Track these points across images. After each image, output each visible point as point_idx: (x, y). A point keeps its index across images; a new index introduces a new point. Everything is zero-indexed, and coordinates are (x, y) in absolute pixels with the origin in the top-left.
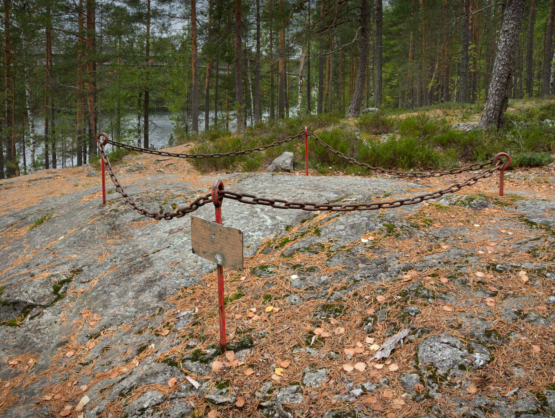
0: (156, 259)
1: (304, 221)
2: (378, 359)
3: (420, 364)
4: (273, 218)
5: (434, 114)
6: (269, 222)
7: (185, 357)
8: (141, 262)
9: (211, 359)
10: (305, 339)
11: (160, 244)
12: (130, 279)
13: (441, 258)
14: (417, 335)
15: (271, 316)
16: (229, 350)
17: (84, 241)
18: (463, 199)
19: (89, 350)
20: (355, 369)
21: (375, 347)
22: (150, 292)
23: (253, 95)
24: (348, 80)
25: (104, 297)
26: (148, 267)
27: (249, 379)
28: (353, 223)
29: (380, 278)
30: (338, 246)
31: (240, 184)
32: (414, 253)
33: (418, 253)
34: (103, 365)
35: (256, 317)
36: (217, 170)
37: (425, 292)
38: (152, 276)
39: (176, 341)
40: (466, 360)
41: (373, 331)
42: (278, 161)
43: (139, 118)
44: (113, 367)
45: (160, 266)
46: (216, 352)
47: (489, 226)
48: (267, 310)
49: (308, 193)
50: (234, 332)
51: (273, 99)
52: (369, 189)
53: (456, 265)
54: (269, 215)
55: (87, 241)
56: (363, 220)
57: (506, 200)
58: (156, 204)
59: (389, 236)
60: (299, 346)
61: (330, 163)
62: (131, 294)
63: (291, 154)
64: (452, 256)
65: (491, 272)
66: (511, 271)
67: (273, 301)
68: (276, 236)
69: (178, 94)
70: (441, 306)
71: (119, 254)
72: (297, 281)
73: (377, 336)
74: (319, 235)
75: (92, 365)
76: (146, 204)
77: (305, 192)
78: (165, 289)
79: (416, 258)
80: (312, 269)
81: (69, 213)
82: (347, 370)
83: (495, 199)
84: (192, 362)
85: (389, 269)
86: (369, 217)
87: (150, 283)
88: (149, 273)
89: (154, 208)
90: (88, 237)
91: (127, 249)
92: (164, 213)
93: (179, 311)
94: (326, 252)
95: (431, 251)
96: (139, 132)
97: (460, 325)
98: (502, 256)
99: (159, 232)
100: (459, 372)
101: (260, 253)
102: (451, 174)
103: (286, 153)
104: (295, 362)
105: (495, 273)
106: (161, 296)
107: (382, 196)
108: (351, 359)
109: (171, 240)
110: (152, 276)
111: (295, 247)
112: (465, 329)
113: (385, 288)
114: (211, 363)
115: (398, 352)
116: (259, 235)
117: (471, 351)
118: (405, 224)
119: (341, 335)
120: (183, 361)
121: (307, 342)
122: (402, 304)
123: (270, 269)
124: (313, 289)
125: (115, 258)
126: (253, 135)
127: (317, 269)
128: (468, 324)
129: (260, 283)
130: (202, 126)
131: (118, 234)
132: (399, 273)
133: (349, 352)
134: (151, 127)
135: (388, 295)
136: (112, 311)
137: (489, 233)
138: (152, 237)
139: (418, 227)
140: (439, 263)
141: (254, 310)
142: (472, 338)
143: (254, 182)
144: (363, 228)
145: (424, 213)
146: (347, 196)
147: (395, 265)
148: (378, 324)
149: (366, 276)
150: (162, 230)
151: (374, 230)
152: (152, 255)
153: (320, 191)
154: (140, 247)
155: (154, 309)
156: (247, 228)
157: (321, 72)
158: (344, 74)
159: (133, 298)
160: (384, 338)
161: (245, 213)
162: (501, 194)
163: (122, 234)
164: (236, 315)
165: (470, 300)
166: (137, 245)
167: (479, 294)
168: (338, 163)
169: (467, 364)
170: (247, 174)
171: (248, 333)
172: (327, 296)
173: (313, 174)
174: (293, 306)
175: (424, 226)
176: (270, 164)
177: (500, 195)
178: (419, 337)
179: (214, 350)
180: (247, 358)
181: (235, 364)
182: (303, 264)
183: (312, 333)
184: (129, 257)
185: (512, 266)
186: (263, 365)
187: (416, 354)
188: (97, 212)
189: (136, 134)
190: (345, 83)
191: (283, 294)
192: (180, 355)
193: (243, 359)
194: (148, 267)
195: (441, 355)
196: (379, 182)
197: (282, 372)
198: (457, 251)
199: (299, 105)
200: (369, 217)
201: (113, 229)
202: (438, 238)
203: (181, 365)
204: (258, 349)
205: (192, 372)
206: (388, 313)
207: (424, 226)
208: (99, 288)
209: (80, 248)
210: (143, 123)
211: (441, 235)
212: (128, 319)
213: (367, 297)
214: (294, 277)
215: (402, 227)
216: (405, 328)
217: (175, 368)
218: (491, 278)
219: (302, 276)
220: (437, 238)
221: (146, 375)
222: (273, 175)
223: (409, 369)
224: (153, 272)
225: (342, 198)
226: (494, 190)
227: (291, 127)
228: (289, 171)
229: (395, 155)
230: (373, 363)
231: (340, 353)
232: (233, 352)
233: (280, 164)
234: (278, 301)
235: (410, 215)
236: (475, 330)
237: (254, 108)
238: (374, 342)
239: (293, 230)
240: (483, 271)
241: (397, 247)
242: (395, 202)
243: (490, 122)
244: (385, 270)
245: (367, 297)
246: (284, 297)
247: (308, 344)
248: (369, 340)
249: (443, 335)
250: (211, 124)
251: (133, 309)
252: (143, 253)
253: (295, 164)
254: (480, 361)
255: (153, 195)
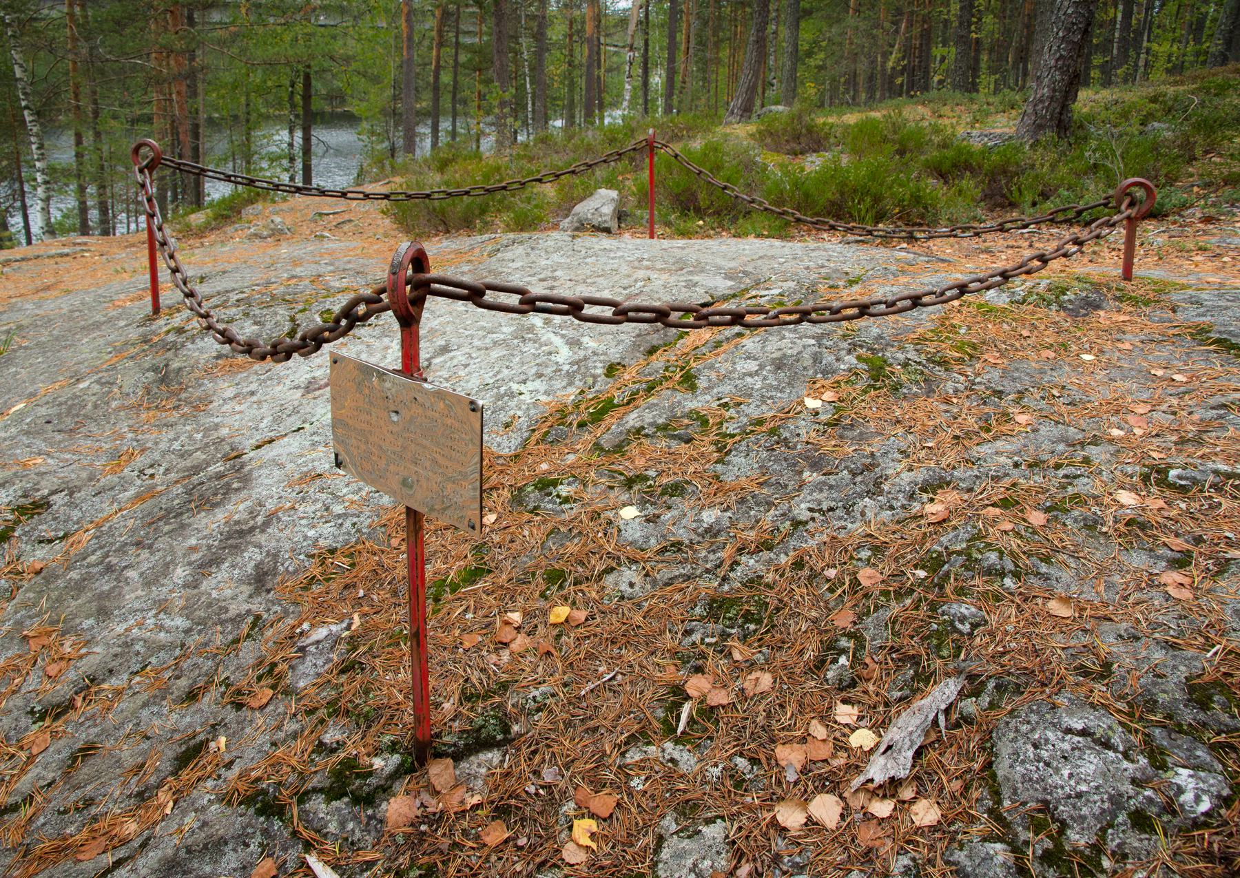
0: (261, 467)
1: (652, 351)
2: (875, 784)
3: (1007, 803)
4: (574, 343)
5: (916, 114)
6: (564, 354)
7: (309, 785)
8: (220, 476)
9: (385, 790)
10: (660, 713)
11: (277, 420)
12: (183, 526)
13: (1018, 453)
14: (985, 700)
15: (564, 638)
16: (439, 755)
17: (77, 415)
18: (1041, 289)
19: (31, 759)
20: (809, 818)
21: (862, 738)
22: (233, 566)
23: (531, 84)
24: (725, 54)
25: (105, 585)
26: (237, 490)
27: (494, 858)
28: (778, 354)
29: (863, 514)
30: (745, 420)
31: (494, 259)
32: (946, 436)
33: (956, 437)
34: (65, 812)
35: (520, 642)
36: (448, 232)
37: (993, 557)
38: (246, 516)
39: (291, 727)
40: (1148, 793)
41: (853, 684)
42: (585, 209)
43: (291, 132)
44: (95, 819)
45: (268, 487)
46: (401, 765)
47: (1119, 359)
48: (552, 619)
49: (659, 279)
50: (457, 696)
51: (571, 90)
52: (807, 268)
53: (1061, 472)
54: (563, 336)
55: (86, 416)
56: (804, 347)
57: (1141, 292)
58: (283, 312)
59: (875, 389)
60: (641, 736)
61: (700, 212)
62: (180, 573)
63: (614, 194)
64: (1046, 446)
65: (1154, 489)
66: (1217, 487)
67: (569, 588)
68: (582, 392)
69: (376, 80)
70: (1040, 601)
71: (163, 454)
72: (636, 524)
73: (865, 698)
74: (693, 388)
75: (30, 811)
76: (258, 312)
77: (654, 276)
78: (276, 556)
79: (953, 454)
80: (677, 489)
81: (57, 339)
82: (788, 824)
83: (1117, 289)
84: (329, 800)
85: (886, 487)
86: (819, 338)
87: (237, 536)
88: (237, 508)
89: (276, 324)
90: (90, 406)
91: (190, 437)
92: (299, 335)
93: (306, 626)
94: (712, 437)
95: (988, 430)
96: (292, 160)
97: (1107, 666)
98: (1176, 443)
99: (280, 388)
100: (1135, 841)
101: (538, 443)
102: (1001, 230)
103: (603, 191)
104: (630, 795)
105: (1168, 493)
106: (260, 580)
107: (841, 283)
108: (796, 783)
109: (308, 409)
110: (246, 516)
111: (631, 423)
112: (1124, 678)
113: (876, 542)
114: (384, 806)
115: (933, 754)
116: (537, 391)
117: (1158, 760)
118: (912, 355)
119: (763, 695)
120: (303, 797)
121: (665, 721)
122: (930, 597)
123: (564, 490)
124: (680, 549)
125: (152, 466)
126: (531, 159)
127: (690, 489)
128: (1128, 661)
129: (531, 534)
130: (425, 146)
131: (174, 394)
132: (911, 497)
133: (791, 757)
134: (317, 149)
135: (889, 568)
136: (120, 629)
137: (1124, 378)
138: (259, 402)
139: (944, 363)
140: (1016, 465)
141: (516, 617)
142: (1151, 711)
143: (528, 254)
144: (805, 368)
145: (954, 326)
146: (757, 284)
147: (900, 476)
148: (868, 660)
149: (825, 508)
150: (288, 382)
151: (834, 372)
152: (252, 454)
153: (691, 273)
154: (224, 432)
155: (237, 620)
156: (506, 371)
157: (672, 37)
158: (717, 45)
159: (185, 586)
160: (886, 705)
161: (505, 329)
162: (1127, 275)
163: (183, 396)
164: (466, 637)
165: (1117, 579)
166: (217, 427)
167: (1138, 560)
168: (718, 213)
169: (1155, 810)
170: (512, 235)
171: (497, 699)
172: (721, 572)
173: (663, 236)
174: (627, 604)
175: (960, 361)
176: (567, 216)
177: (1125, 279)
178: (992, 705)
179: (396, 759)
180: (491, 780)
181: (453, 802)
182: (652, 473)
183: (679, 694)
184: (188, 463)
185: (1216, 472)
186: (538, 806)
187: (988, 765)
188: (134, 334)
189: (285, 162)
190: (718, 62)
191: (600, 567)
192: (292, 778)
193: (480, 782)
194: (237, 490)
195: (1071, 776)
196: (825, 250)
197: (593, 836)
198: (1057, 431)
199: (625, 104)
200: (819, 338)
201: (163, 380)
202: (1001, 392)
203: (295, 811)
204: (525, 751)
205: (325, 836)
206: (894, 623)
207: (960, 361)
208: (93, 559)
209: (59, 437)
210: (301, 141)
211: (1008, 386)
212: (162, 654)
213: (831, 573)
214: (630, 512)
215: (905, 365)
216: (948, 675)
217: (277, 824)
218: (1160, 510)
219: (651, 510)
220: (999, 394)
221: (189, 851)
222: (574, 237)
223: (973, 820)
224: (248, 503)
225: (746, 290)
226: (1107, 265)
227: (612, 141)
228: (607, 231)
229: (842, 194)
230: (862, 796)
231: (763, 760)
232: (449, 761)
233: (589, 216)
234: (583, 587)
235: (920, 330)
236: (1154, 684)
237: (533, 111)
238: (860, 718)
239: (626, 377)
240: (1133, 489)
241: (898, 422)
242: (873, 304)
243: (1040, 127)
244: (875, 489)
245: (831, 573)
246: (600, 577)
247: (670, 730)
248: (845, 713)
249: (1062, 700)
250: (444, 139)
251: (180, 622)
252: (227, 448)
253: (621, 216)
254: (1198, 799)
255: (279, 290)
